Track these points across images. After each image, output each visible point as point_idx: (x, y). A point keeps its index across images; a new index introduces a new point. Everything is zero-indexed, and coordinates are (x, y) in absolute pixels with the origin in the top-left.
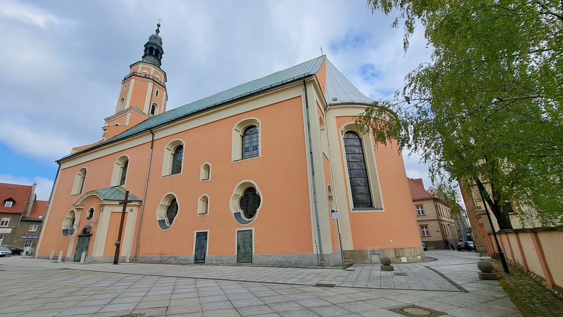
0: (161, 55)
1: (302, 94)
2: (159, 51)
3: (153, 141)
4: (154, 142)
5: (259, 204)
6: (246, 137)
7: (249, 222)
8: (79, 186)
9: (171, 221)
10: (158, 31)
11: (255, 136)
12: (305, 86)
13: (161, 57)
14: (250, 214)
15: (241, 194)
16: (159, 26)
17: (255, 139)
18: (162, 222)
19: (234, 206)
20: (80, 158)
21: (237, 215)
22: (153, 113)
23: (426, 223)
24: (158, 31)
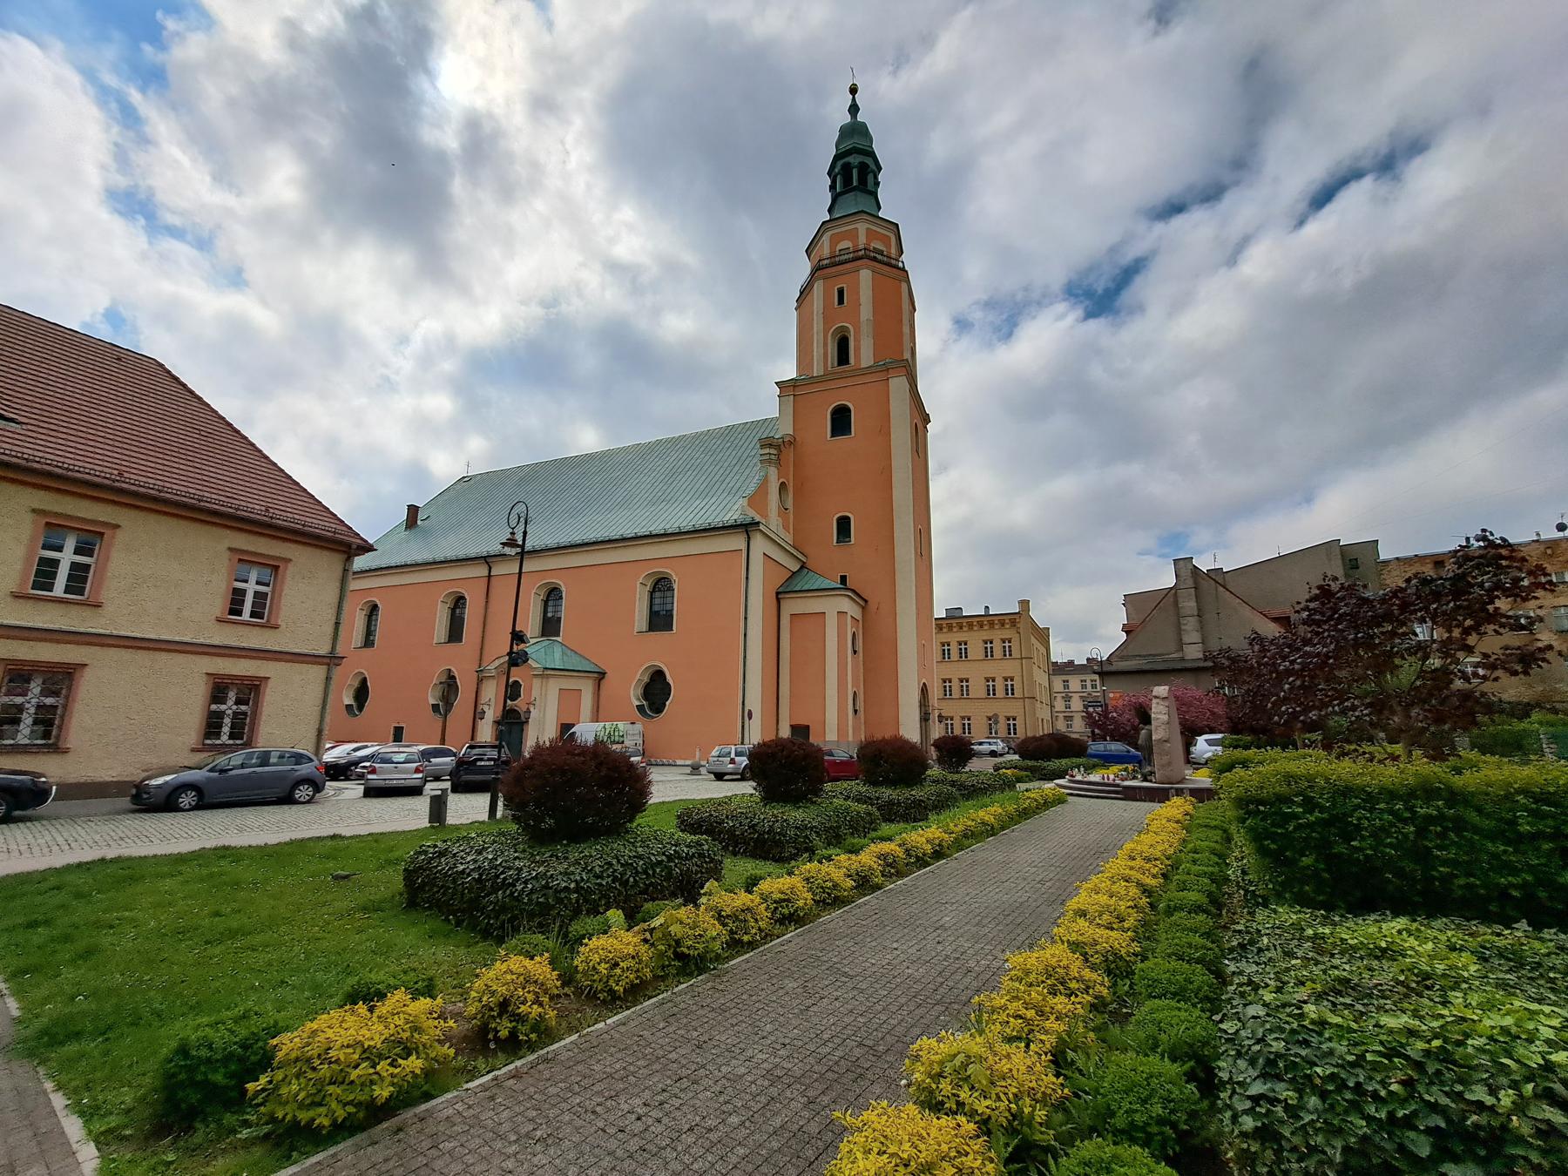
0: (876, 177)
1: (743, 546)
2: (868, 166)
3: (489, 576)
4: (492, 578)
5: (669, 694)
6: (657, 594)
7: (653, 718)
8: (376, 625)
9: (361, 708)
10: (854, 109)
11: (669, 594)
12: (749, 538)
13: (877, 184)
14: (658, 709)
15: (646, 679)
16: (853, 90)
17: (669, 600)
18: (349, 707)
19: (635, 698)
20: (274, 541)
21: (640, 708)
22: (843, 357)
23: (1070, 714)
24: (854, 109)
